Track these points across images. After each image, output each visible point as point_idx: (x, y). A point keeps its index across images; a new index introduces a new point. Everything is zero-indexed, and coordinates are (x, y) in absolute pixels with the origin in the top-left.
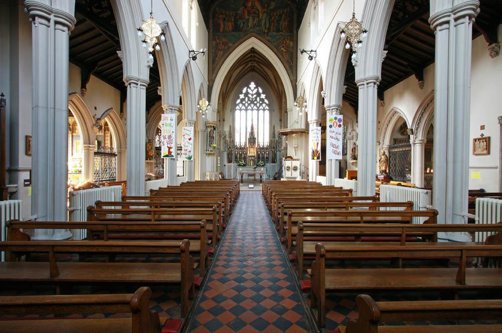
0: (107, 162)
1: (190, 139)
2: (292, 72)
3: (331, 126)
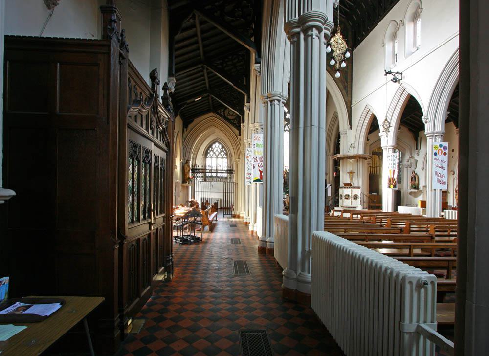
2: (347, 93)
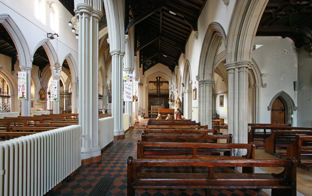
0: (6, 102)
1: (55, 88)
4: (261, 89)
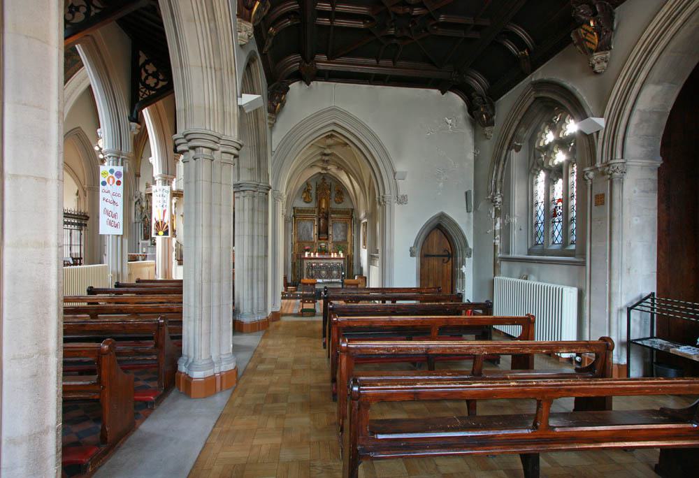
3: (104, 183)
4: (397, 207)
